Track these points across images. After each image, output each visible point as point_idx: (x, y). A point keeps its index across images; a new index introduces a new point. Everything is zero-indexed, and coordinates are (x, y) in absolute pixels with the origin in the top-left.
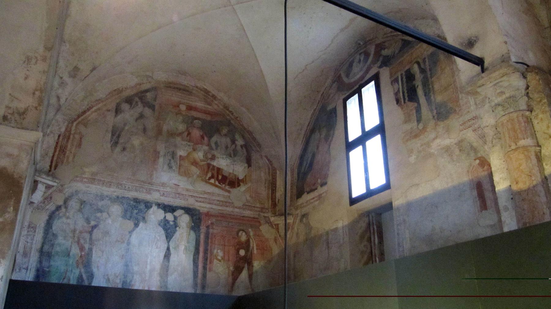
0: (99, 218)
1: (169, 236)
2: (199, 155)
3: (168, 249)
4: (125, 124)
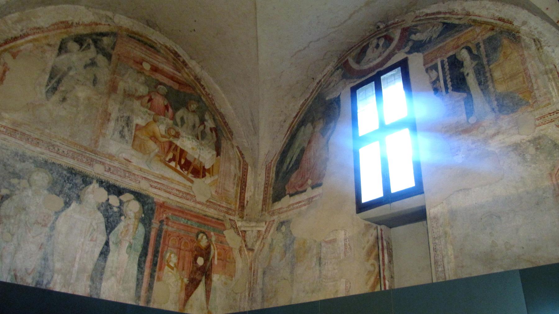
0: (14, 186)
1: (110, 227)
2: (161, 129)
3: (107, 244)
4: (70, 69)
